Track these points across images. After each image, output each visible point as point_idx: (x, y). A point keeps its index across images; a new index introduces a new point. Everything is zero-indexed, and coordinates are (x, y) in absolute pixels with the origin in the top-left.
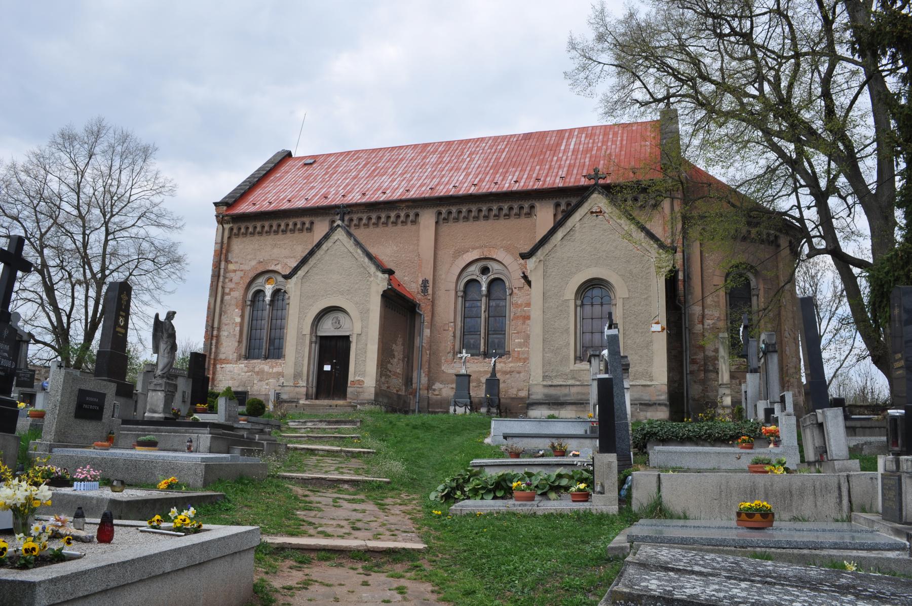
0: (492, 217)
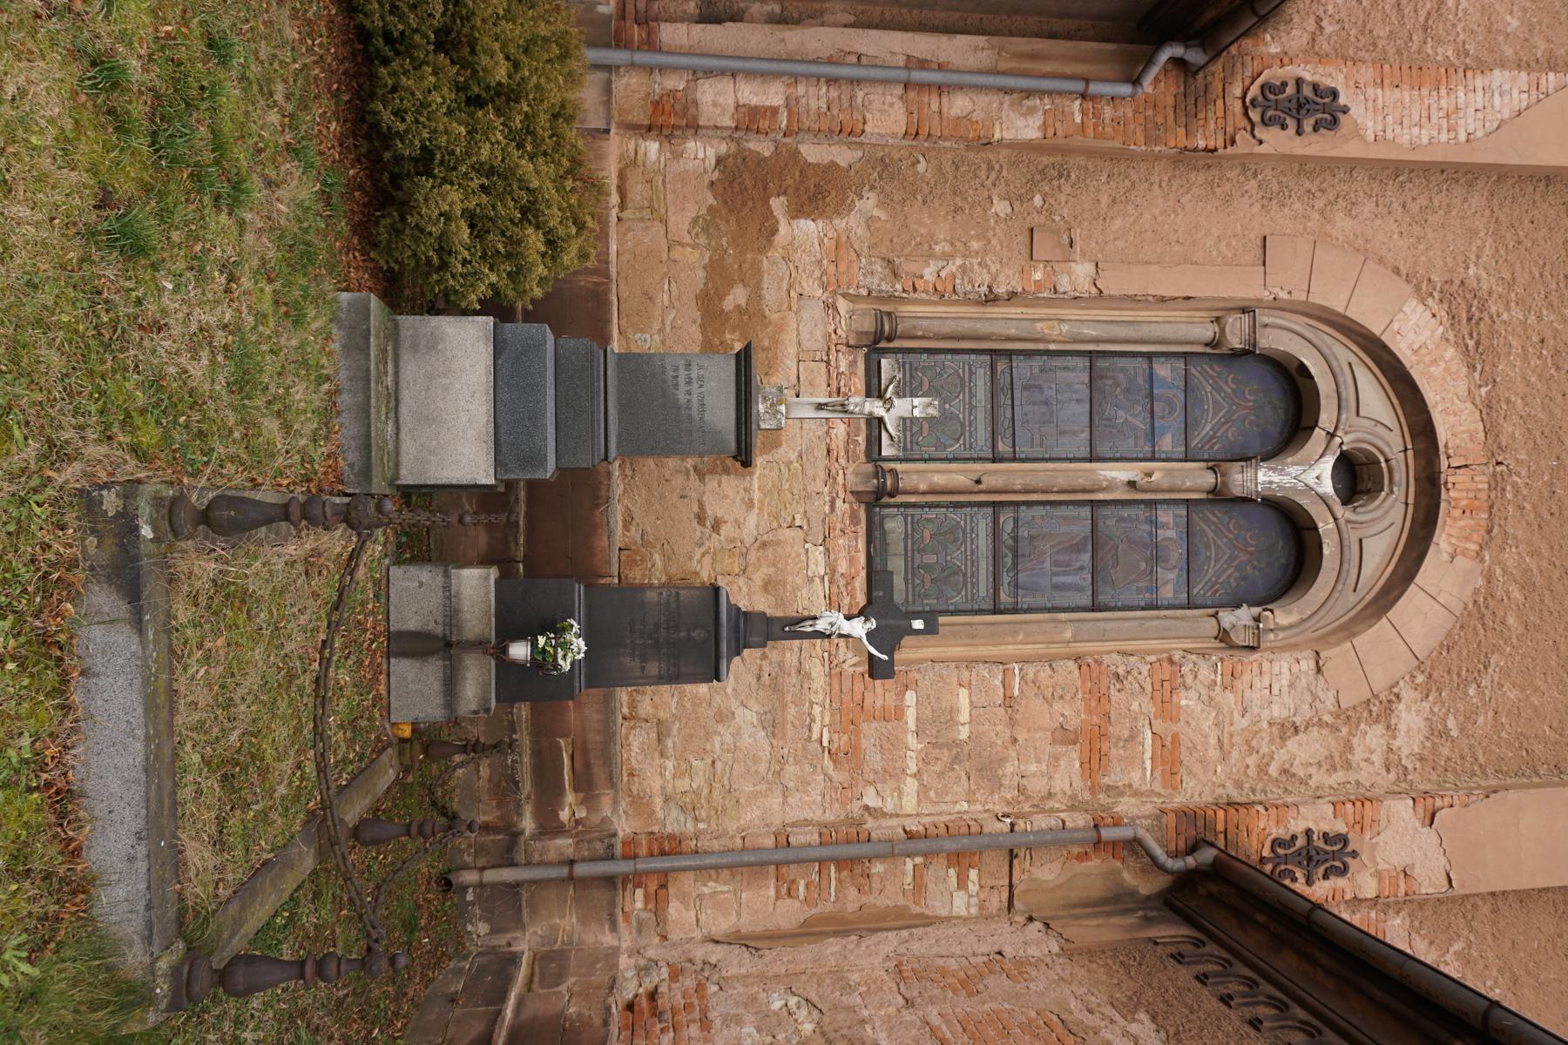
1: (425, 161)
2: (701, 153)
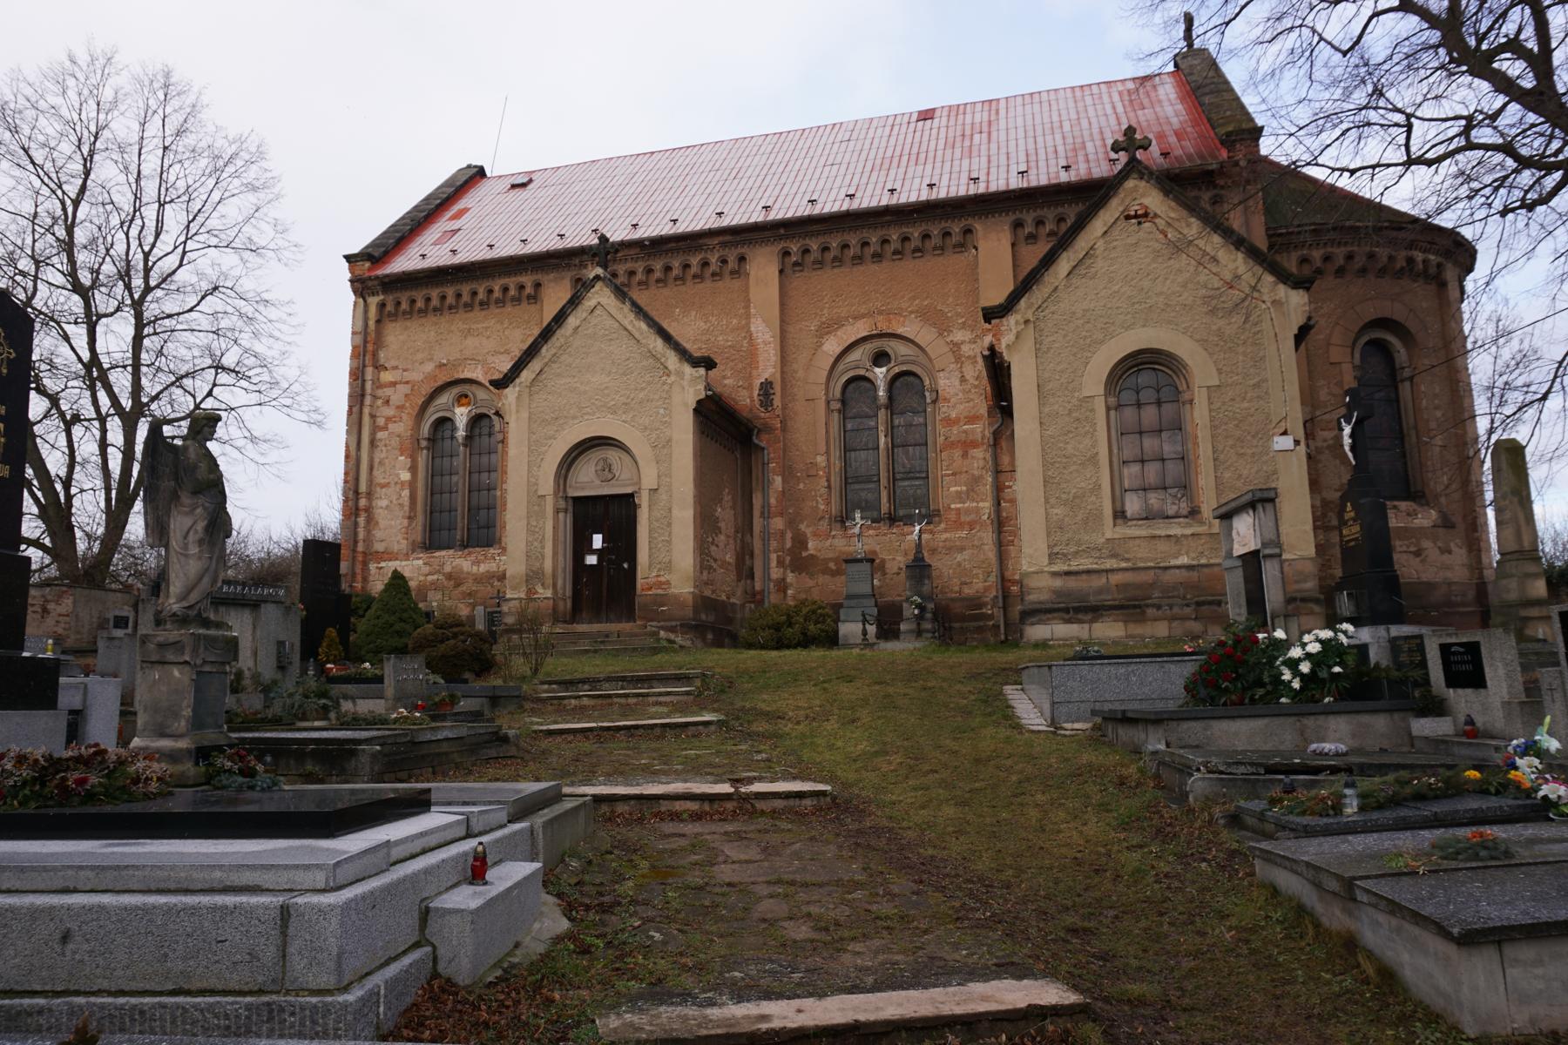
0: (889, 254)
1: (804, 634)
2: (790, 577)
